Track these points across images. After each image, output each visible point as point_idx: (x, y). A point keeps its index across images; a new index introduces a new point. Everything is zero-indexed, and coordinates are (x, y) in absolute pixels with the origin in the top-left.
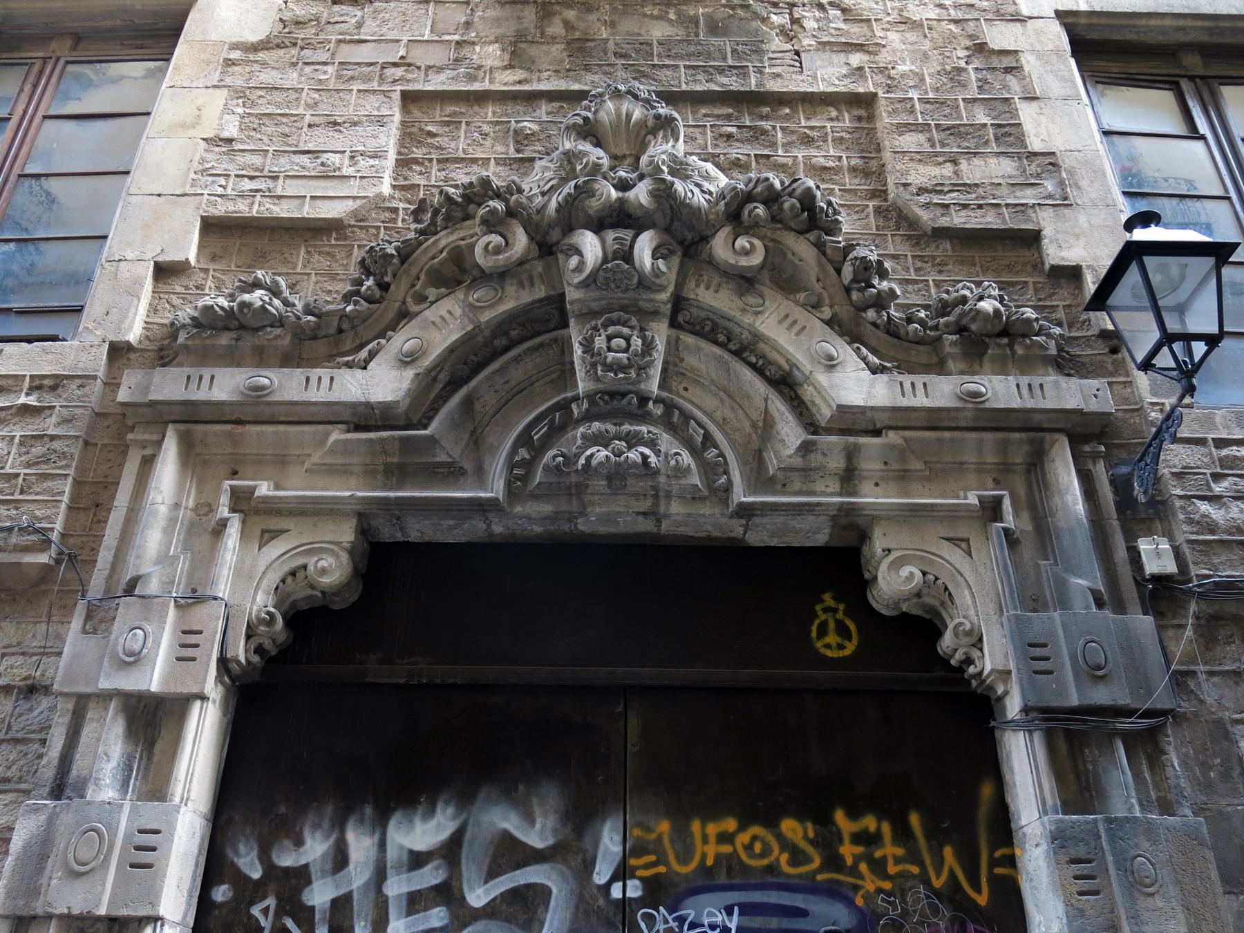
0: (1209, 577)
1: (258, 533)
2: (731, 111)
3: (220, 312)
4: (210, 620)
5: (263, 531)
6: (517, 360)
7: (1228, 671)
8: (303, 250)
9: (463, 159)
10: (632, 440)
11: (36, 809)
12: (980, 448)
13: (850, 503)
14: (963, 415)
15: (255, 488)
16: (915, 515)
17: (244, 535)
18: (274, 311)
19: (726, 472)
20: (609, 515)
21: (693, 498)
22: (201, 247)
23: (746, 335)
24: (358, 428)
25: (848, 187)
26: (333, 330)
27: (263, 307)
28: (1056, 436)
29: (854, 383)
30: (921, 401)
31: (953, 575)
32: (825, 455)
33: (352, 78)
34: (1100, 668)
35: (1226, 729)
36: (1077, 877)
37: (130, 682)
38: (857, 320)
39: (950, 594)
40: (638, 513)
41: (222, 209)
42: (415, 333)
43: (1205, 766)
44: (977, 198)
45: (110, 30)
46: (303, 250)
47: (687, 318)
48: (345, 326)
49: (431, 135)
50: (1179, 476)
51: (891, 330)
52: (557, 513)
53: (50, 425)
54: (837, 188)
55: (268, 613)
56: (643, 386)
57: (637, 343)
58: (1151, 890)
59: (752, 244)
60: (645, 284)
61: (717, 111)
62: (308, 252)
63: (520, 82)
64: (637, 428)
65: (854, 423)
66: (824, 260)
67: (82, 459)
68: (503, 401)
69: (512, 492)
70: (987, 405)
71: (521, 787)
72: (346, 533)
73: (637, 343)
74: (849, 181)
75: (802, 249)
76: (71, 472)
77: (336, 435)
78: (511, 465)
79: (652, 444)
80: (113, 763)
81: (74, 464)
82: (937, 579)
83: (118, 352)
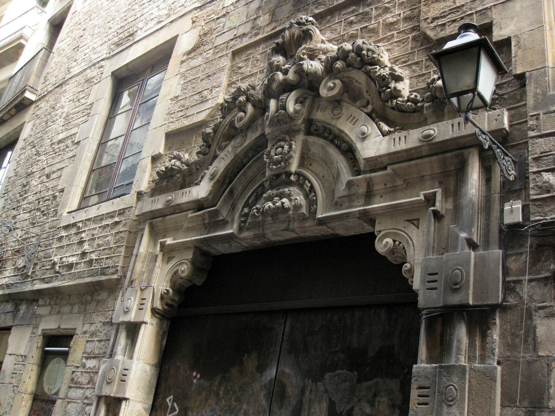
0: (541, 220)
1: (167, 258)
2: (354, 7)
3: (162, 173)
4: (148, 295)
5: (169, 258)
6: (249, 167)
7: (541, 278)
8: (194, 137)
9: (249, 76)
10: (281, 196)
11: (104, 362)
12: (431, 166)
13: (365, 210)
14: (424, 148)
15: (166, 241)
16: (393, 212)
17: (163, 260)
18: (176, 168)
19: (316, 204)
20: (276, 233)
21: (303, 219)
22: (166, 145)
23: (337, 132)
24: (199, 210)
25: (402, 30)
26: (195, 170)
27: (171, 167)
28: (470, 150)
29: (375, 143)
30: (402, 146)
31: (407, 240)
32: (358, 186)
33: (218, 52)
34: (456, 284)
35: (531, 313)
36: (419, 396)
37: (126, 319)
38: (384, 107)
39: (405, 251)
40: (283, 230)
41: (174, 127)
42: (216, 165)
43: (514, 335)
44: (461, 14)
45: (161, 60)
46: (194, 137)
47: (315, 128)
48: (198, 167)
49: (240, 68)
50: (536, 159)
51: (399, 109)
52: (255, 235)
53: (120, 228)
54: (395, 32)
55: (166, 290)
56: (287, 169)
57: (286, 147)
58: (451, 403)
59: (334, 84)
60: (291, 118)
61: (350, 10)
62: (196, 137)
63: (273, 29)
64: (281, 190)
65: (376, 166)
66: (369, 80)
67: (128, 237)
68: (244, 187)
69: (241, 229)
70: (433, 141)
71: (246, 355)
72: (189, 255)
73: (286, 147)
74: (402, 26)
75: (359, 77)
76: (124, 244)
77: (190, 215)
78: (241, 216)
79: (289, 196)
80: (122, 347)
81: (125, 241)
82: (400, 243)
83: (140, 195)
